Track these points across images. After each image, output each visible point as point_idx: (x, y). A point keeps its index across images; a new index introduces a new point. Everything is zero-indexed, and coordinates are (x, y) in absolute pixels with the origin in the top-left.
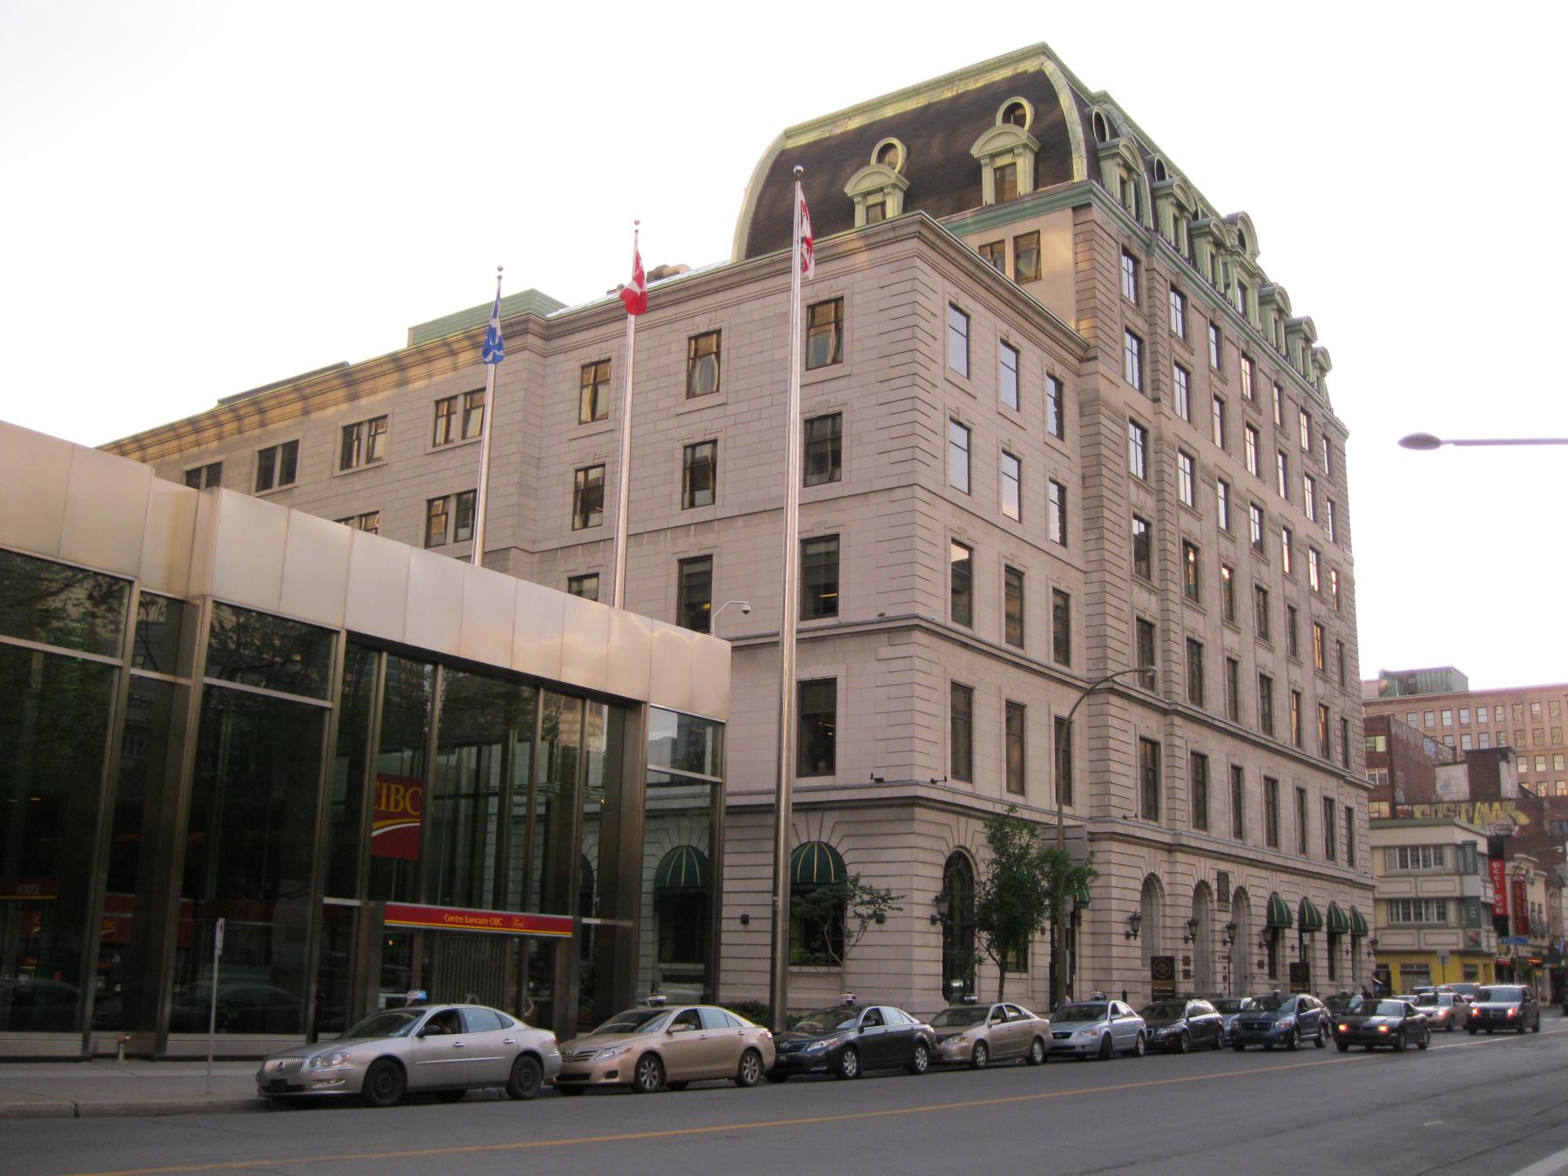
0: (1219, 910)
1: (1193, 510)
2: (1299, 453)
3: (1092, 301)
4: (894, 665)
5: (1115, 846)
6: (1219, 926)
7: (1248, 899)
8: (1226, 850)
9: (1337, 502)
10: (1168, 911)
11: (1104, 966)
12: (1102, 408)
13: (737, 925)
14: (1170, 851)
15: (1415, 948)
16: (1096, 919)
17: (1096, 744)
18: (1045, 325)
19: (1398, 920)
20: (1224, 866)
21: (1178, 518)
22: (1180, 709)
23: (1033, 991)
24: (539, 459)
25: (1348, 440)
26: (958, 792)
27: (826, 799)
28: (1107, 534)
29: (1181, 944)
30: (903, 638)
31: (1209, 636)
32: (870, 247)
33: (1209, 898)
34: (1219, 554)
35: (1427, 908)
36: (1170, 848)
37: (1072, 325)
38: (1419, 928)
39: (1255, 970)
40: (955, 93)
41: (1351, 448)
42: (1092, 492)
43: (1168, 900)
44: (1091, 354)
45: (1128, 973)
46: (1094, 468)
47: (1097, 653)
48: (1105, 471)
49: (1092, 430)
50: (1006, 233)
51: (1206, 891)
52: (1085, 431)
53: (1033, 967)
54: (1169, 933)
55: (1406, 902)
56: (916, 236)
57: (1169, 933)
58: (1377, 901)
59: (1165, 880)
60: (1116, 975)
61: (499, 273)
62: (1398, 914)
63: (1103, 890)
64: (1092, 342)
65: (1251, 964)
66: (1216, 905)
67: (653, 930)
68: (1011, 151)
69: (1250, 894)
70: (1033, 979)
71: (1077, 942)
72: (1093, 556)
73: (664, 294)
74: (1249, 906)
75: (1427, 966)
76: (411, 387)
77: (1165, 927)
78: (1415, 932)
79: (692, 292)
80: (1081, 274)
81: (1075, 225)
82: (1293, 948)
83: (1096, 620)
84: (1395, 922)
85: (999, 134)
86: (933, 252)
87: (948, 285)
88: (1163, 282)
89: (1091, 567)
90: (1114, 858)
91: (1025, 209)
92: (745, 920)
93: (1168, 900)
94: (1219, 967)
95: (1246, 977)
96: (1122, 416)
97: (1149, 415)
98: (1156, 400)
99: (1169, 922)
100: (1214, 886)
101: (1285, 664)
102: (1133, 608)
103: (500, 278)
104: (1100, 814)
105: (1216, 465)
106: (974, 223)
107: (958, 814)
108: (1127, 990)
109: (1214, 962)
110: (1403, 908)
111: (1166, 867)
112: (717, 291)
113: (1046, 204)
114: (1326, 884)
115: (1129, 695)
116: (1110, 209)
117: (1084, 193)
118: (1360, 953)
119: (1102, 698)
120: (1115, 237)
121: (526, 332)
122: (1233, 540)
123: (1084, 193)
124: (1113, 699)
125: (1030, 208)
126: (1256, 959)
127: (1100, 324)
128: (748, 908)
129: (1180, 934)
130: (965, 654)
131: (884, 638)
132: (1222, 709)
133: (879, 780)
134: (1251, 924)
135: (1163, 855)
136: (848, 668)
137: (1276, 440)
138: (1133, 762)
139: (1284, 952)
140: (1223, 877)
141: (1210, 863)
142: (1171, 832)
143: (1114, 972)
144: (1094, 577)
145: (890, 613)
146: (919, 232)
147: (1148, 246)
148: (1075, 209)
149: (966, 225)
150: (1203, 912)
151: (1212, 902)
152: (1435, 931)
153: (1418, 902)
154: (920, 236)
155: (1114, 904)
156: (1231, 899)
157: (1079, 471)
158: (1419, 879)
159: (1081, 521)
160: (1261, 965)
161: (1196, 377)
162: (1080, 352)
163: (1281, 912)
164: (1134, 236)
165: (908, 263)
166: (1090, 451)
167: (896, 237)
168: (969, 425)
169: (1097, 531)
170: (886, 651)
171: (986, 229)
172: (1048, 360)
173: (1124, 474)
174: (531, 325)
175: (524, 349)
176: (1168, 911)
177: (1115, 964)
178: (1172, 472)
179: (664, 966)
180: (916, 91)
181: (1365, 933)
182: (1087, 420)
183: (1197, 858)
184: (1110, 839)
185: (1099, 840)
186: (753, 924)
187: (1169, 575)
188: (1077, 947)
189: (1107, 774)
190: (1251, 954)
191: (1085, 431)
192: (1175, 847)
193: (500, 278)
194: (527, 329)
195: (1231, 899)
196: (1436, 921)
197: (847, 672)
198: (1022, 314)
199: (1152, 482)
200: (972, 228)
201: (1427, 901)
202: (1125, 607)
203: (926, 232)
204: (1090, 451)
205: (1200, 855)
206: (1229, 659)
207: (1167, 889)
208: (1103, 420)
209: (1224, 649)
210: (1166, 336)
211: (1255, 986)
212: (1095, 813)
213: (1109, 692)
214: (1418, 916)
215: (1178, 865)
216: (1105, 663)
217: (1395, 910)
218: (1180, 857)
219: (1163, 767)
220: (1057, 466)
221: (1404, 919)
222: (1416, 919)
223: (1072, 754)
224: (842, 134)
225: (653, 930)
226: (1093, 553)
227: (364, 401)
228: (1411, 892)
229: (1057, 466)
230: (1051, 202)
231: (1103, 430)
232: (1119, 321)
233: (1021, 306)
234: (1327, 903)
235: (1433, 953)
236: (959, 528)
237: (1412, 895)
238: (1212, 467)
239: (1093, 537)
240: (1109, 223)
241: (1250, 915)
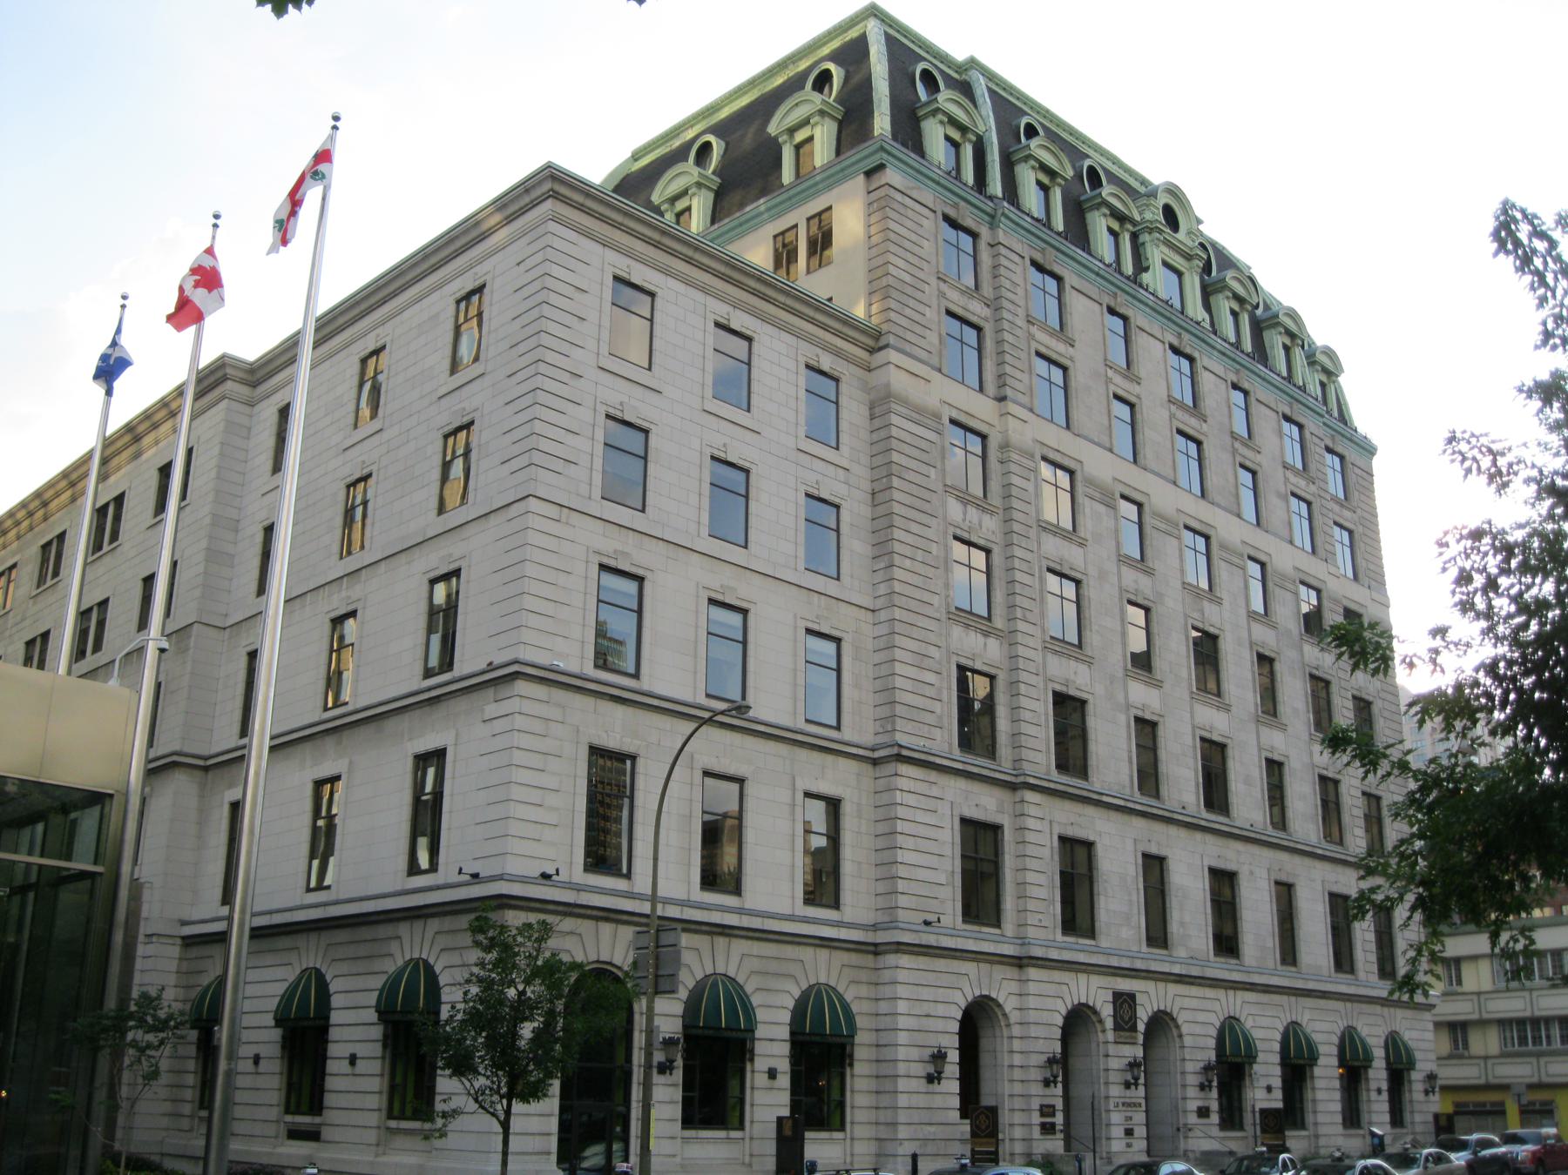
0: (1116, 1042)
1: (1072, 535)
2: (1281, 470)
3: (884, 279)
4: (499, 725)
5: (905, 960)
6: (1114, 1064)
7: (1178, 1027)
8: (1126, 963)
9: (1358, 530)
10: (1017, 1045)
11: (889, 1121)
12: (893, 405)
13: (344, 1066)
14: (1020, 967)
15: (1482, 1081)
16: (881, 1058)
17: (882, 828)
18: (798, 306)
19: (1513, 1045)
20: (1125, 985)
21: (1039, 544)
22: (1032, 781)
23: (751, 1155)
24: (238, 521)
25: (1375, 458)
26: (603, 889)
27: (422, 903)
28: (897, 560)
29: (1037, 1089)
30: (505, 691)
31: (1099, 689)
32: (510, 220)
33: (1099, 1027)
34: (1120, 588)
35: (1547, 1029)
36: (1020, 963)
37: (859, 312)
38: (1539, 1055)
39: (1193, 1119)
40: (786, 78)
41: (1380, 465)
42: (881, 510)
43: (1016, 1031)
44: (882, 342)
45: (932, 1129)
46: (884, 480)
47: (884, 712)
48: (896, 482)
49: (883, 434)
50: (798, 216)
51: (1094, 1018)
52: (875, 437)
53: (752, 1122)
54: (1017, 1074)
55: (1521, 1022)
56: (550, 196)
57: (1017, 1074)
58: (1438, 1025)
59: (1009, 1004)
60: (903, 1133)
61: (122, 302)
62: (1513, 1038)
63: (888, 1018)
64: (885, 328)
65: (1185, 1111)
66: (1110, 1036)
67: (281, 1074)
68: (805, 122)
69: (1180, 1021)
70: (852, 1139)
71: (748, 1085)
72: (883, 589)
73: (342, 313)
74: (1180, 1036)
75: (1551, 1102)
76: (145, 457)
77: (1011, 1066)
78: (1534, 1060)
79: (364, 306)
80: (874, 250)
81: (869, 193)
82: (1379, 1091)
83: (884, 670)
84: (1510, 1048)
85: (797, 104)
86: (583, 215)
87: (611, 255)
88: (1017, 258)
89: (879, 603)
90: (902, 976)
91: (816, 184)
92: (353, 1060)
93: (1016, 1031)
94: (1116, 1118)
95: (1178, 1130)
96: (937, 416)
97: (995, 420)
98: (1002, 399)
99: (1017, 1060)
100: (1107, 1011)
101: (1252, 726)
102: (950, 653)
103: (123, 307)
104: (887, 919)
105: (1115, 479)
106: (768, 210)
107: (597, 919)
108: (918, 1152)
109: (1108, 1111)
110: (1518, 1031)
111: (1014, 987)
112: (384, 302)
113: (837, 173)
114: (1283, 999)
115: (934, 763)
116: (918, 171)
117: (876, 152)
118: (1368, 1090)
119: (889, 768)
120: (931, 206)
121: (224, 379)
122: (1149, 572)
123: (876, 152)
124: (904, 769)
125: (823, 180)
126: (1193, 1105)
127: (893, 305)
128: (358, 1044)
129: (1036, 1075)
130: (620, 711)
131: (490, 693)
132: (1127, 782)
133: (475, 876)
134: (1184, 1060)
135: (1011, 972)
136: (457, 735)
137: (1234, 452)
138: (947, 851)
139: (1369, 1096)
140: (1125, 1002)
141: (1097, 981)
142: (1019, 941)
143: (901, 1128)
144: (883, 615)
145: (497, 661)
146: (552, 190)
147: (993, 217)
148: (869, 174)
149: (761, 214)
150: (1094, 1045)
151: (1104, 1031)
152: (1560, 1059)
153: (1536, 1022)
154: (555, 195)
155: (902, 1038)
156: (1141, 1027)
157: (867, 486)
158: (1535, 994)
159: (870, 547)
160: (1203, 1112)
161: (1079, 377)
162: (870, 342)
163: (1236, 1043)
164: (962, 204)
165: (540, 230)
166: (879, 460)
167: (532, 202)
168: (645, 425)
169: (886, 558)
170: (492, 710)
171: (779, 215)
172: (809, 352)
173: (939, 488)
174: (229, 371)
175: (223, 398)
176: (1017, 1045)
177: (902, 1117)
178: (1030, 486)
179: (289, 1118)
180: (752, 83)
181: (1411, 1065)
182: (877, 423)
183: (1073, 975)
184: (897, 952)
185: (885, 952)
186: (361, 1066)
187: (1019, 613)
188: (848, 1094)
189: (894, 866)
190: (1184, 1099)
191: (875, 437)
192: (1025, 961)
193: (123, 307)
194: (225, 375)
195: (1141, 1027)
196: (1559, 1045)
197: (456, 739)
198: (755, 293)
199: (995, 499)
200: (766, 216)
201: (1548, 1021)
202: (933, 651)
203: (557, 187)
204: (879, 460)
205: (1077, 971)
206: (1138, 720)
207: (1014, 1017)
208: (895, 419)
209: (1128, 706)
210: (1021, 322)
211: (1190, 1141)
212: (881, 917)
213: (897, 760)
214: (1537, 1040)
215: (1030, 983)
216: (894, 723)
217: (1508, 1035)
218: (1033, 973)
219: (1007, 857)
220: (820, 477)
221: (1520, 1045)
222: (1534, 1043)
223: (841, 842)
224: (681, 145)
225: (281, 1074)
226: (882, 585)
227: (112, 479)
228: (1473, 1013)
229: (820, 477)
230: (842, 170)
231: (895, 432)
232: (934, 303)
233: (752, 283)
234: (1338, 1026)
235: (1505, 1088)
236: (615, 551)
237: (1528, 1014)
238: (1109, 480)
239: (882, 565)
240: (913, 188)
241: (1183, 1047)
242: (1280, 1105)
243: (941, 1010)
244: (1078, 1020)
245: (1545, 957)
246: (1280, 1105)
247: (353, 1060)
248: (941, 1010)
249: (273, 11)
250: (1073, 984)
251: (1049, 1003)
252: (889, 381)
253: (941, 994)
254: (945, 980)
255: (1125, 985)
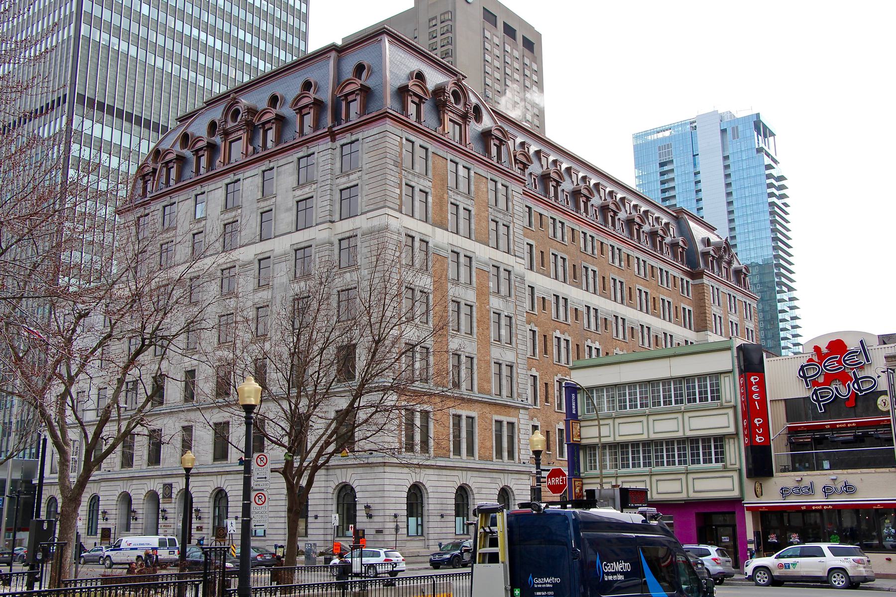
69: (513, 489)
92: (316, 517)
141: (157, 481)
242: (177, 557)
243: (111, 498)
244: (153, 496)
245: (705, 380)
246: (177, 557)
247: (316, 517)
248: (111, 498)
249: (820, 348)
250: (148, 483)
251: (140, 491)
252: (879, 336)
253: (202, 489)
254: (113, 488)
255: (168, 481)
